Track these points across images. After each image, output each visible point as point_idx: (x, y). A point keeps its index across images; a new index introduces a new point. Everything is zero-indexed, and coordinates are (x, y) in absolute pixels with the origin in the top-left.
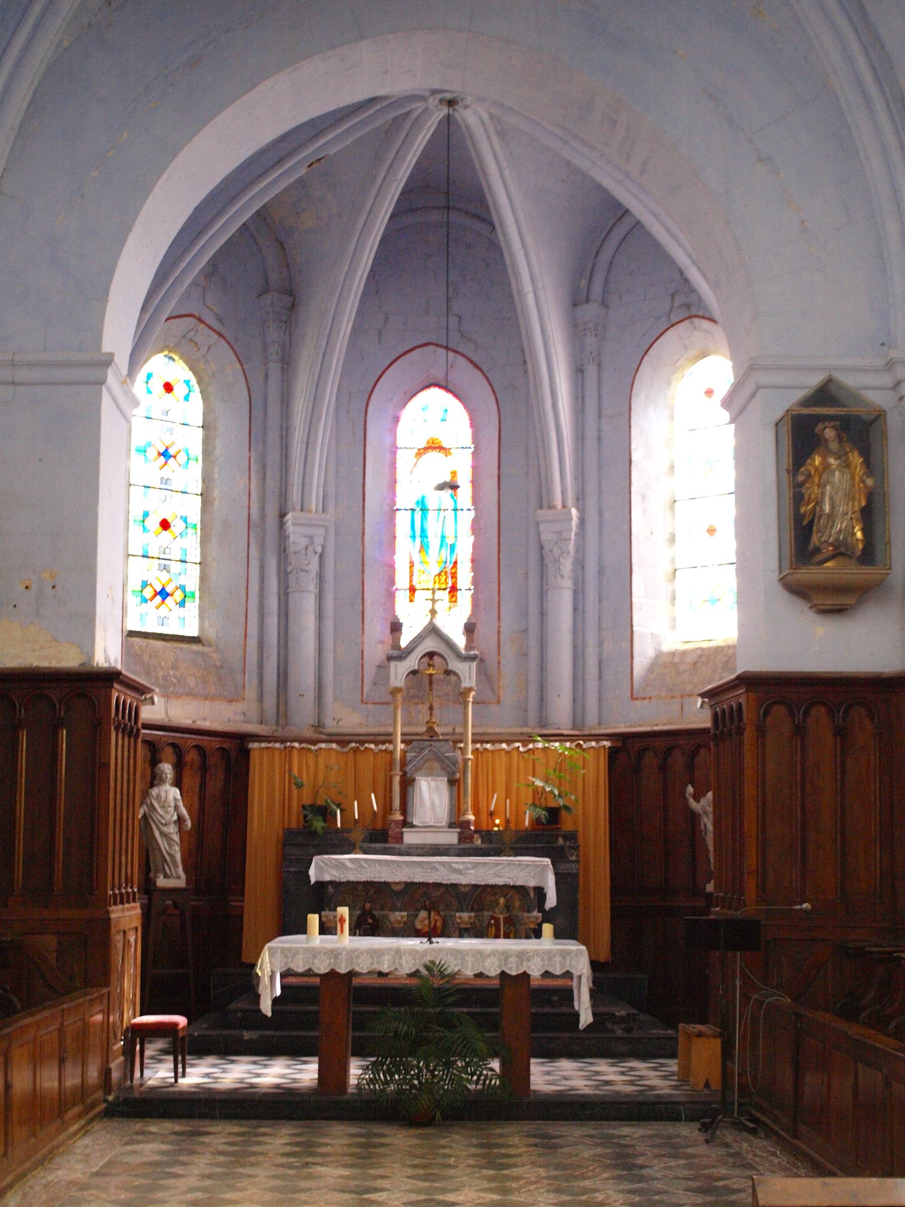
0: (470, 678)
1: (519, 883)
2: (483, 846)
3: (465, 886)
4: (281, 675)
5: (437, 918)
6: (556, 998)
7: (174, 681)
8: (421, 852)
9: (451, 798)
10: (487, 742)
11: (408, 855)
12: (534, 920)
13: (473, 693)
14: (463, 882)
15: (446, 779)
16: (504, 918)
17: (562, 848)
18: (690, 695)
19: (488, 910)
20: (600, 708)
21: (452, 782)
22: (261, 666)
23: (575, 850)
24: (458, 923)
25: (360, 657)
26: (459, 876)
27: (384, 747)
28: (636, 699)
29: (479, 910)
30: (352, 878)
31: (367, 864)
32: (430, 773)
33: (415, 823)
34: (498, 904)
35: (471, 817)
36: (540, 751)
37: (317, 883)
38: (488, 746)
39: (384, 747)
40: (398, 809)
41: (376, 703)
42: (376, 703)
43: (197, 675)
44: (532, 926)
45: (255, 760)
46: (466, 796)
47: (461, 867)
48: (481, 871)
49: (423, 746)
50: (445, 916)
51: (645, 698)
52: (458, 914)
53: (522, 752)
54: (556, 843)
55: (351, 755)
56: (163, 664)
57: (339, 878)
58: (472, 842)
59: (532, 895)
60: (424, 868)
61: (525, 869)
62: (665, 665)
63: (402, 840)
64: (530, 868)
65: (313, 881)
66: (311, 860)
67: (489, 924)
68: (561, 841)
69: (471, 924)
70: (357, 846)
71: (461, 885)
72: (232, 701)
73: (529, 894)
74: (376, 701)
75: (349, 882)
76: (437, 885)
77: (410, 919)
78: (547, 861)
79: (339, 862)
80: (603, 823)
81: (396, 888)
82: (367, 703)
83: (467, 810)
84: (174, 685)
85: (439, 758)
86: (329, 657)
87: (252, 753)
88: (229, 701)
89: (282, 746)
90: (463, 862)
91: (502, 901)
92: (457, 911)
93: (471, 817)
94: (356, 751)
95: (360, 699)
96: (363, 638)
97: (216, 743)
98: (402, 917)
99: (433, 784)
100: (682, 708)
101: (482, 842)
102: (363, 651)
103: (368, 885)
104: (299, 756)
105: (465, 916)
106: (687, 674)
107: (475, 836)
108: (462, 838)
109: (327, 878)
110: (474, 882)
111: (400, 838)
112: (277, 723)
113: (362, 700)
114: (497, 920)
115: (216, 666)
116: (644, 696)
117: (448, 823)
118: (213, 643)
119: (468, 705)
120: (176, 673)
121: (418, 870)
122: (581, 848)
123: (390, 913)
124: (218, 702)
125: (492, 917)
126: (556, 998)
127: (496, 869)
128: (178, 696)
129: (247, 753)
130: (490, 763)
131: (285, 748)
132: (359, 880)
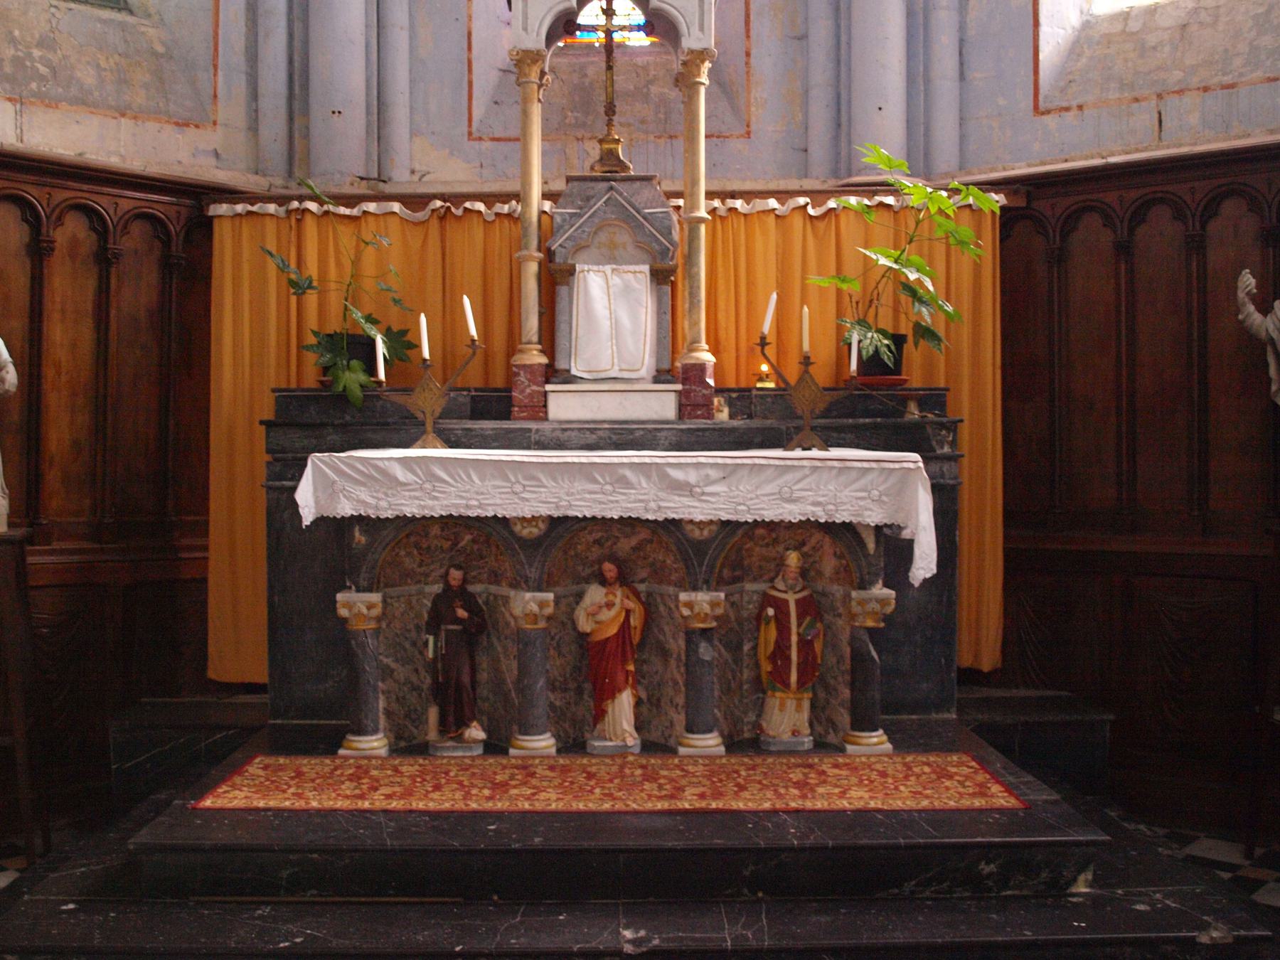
0: (702, 28)
1: (840, 518)
2: (736, 423)
3: (700, 524)
4: (296, 77)
5: (631, 604)
6: (992, 868)
7: (43, 70)
8: (592, 438)
9: (660, 313)
10: (733, 195)
11: (560, 446)
12: (877, 607)
13: (707, 65)
14: (698, 517)
15: (646, 268)
16: (798, 602)
17: (919, 426)
18: (1180, 92)
19: (755, 580)
20: (963, 138)
21: (661, 277)
22: (253, 56)
23: (948, 430)
24: (683, 617)
25: (465, 46)
26: (687, 501)
27: (506, 209)
28: (1048, 112)
29: (736, 580)
30: (411, 510)
31: (446, 470)
32: (611, 257)
33: (574, 372)
34: (781, 563)
35: (707, 357)
36: (852, 215)
37: (320, 521)
38: (738, 204)
39: (506, 209)
40: (535, 338)
41: (498, 140)
42: (498, 140)
43: (103, 64)
44: (870, 623)
45: (223, 236)
46: (694, 304)
47: (692, 477)
48: (744, 487)
49: (592, 193)
50: (649, 594)
51: (1067, 109)
52: (683, 596)
53: (811, 217)
54: (902, 414)
55: (435, 223)
56: (17, 33)
57: (377, 508)
58: (710, 416)
59: (871, 545)
60: (596, 481)
61: (857, 480)
62: (1108, 39)
63: (546, 413)
64: (870, 477)
65: (308, 517)
66: (305, 460)
67: (759, 617)
68: (914, 412)
69: (717, 618)
70: (429, 427)
71: (691, 521)
72: (187, 125)
73: (862, 543)
74: (497, 135)
75: (403, 521)
76: (630, 524)
77: (563, 607)
78: (913, 459)
79: (377, 468)
80: (989, 369)
81: (527, 532)
82: (480, 139)
83: (696, 341)
84: (42, 78)
85: (630, 218)
86: (399, 41)
87: (216, 225)
88: (177, 124)
89: (282, 211)
90: (698, 466)
91: (793, 558)
92: (682, 586)
93: (707, 357)
94: (444, 216)
95: (466, 129)
96: (469, 8)
97: (130, 200)
98: (542, 605)
99: (616, 280)
100: (1160, 122)
101: (731, 417)
102: (470, 34)
103: (452, 524)
104: (319, 234)
105: (703, 598)
106: (1167, 49)
107: (716, 401)
108: (684, 409)
109: (346, 509)
110: (725, 517)
111: (539, 409)
112: (290, 174)
113: (470, 134)
114: (781, 606)
115: (155, 54)
116: (1065, 104)
117: (654, 373)
118: (152, 10)
119: (697, 93)
120: (50, 56)
121: (580, 485)
122: (965, 431)
123: (512, 593)
124: (152, 126)
125: (767, 600)
126: (992, 868)
127: (780, 481)
128: (50, 103)
129: (205, 226)
130: (743, 237)
131: (289, 212)
132: (427, 513)
